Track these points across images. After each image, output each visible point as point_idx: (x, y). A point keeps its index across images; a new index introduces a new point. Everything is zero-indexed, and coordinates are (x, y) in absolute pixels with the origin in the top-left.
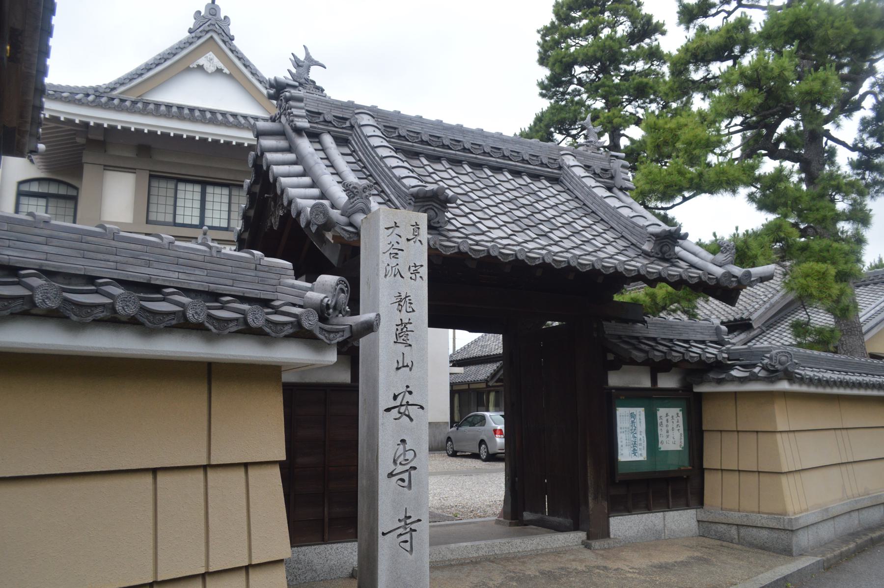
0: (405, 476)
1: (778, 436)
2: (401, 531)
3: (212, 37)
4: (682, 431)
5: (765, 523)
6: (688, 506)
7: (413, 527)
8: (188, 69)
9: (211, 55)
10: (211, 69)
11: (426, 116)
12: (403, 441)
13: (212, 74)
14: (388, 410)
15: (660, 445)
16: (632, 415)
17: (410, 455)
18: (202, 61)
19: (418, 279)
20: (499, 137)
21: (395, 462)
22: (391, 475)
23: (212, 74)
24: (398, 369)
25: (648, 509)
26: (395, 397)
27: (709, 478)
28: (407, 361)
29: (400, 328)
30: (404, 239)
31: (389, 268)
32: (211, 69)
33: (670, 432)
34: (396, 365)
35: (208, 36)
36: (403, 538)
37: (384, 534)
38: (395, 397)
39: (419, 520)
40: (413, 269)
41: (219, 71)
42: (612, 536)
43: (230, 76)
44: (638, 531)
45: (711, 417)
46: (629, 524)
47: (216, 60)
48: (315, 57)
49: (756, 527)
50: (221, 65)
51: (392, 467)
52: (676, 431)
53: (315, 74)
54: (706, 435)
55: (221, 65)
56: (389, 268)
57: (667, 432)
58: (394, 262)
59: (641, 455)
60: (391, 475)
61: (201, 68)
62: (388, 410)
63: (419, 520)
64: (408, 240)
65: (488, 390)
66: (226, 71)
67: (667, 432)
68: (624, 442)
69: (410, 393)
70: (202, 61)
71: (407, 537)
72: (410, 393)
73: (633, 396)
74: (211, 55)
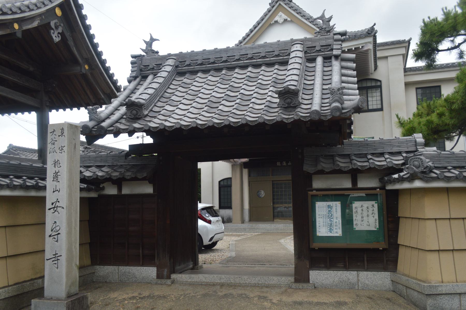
0: (56, 237)
1: (428, 222)
2: (53, 259)
3: (280, 4)
4: (376, 216)
5: (417, 288)
6: (385, 269)
7: (59, 258)
8: (271, 25)
9: (281, 13)
10: (281, 21)
11: (184, 51)
12: (55, 222)
13: (283, 23)
14: (50, 209)
15: (355, 226)
16: (329, 207)
17: (58, 228)
18: (277, 18)
19: (63, 152)
20: (227, 50)
21: (52, 230)
22: (50, 236)
23: (283, 23)
24: (54, 192)
25: (346, 268)
26: (52, 204)
27: (402, 251)
28: (58, 189)
29: (55, 174)
30: (57, 136)
31: (51, 150)
32: (281, 21)
33: (365, 218)
34: (53, 191)
35: (278, 4)
36: (54, 262)
37: (47, 260)
38: (52, 204)
39: (61, 256)
40: (61, 148)
41: (285, 20)
42: (311, 282)
43: (291, 21)
44: (334, 281)
45: (406, 208)
46: (325, 276)
47: (283, 15)
48: (154, 37)
49: (442, 294)
50: (286, 17)
51: (51, 233)
52: (371, 216)
53: (155, 47)
54: (401, 220)
55: (286, 17)
56: (51, 150)
57: (362, 217)
58: (53, 146)
59: (337, 232)
60: (50, 236)
61: (276, 22)
62: (50, 209)
63: (61, 256)
64: (59, 136)
65: (387, 182)
66: (289, 19)
67: (362, 217)
68: (322, 224)
69: (59, 202)
70: (277, 18)
71: (56, 262)
72: (59, 202)
73: (329, 195)
74: (281, 13)
